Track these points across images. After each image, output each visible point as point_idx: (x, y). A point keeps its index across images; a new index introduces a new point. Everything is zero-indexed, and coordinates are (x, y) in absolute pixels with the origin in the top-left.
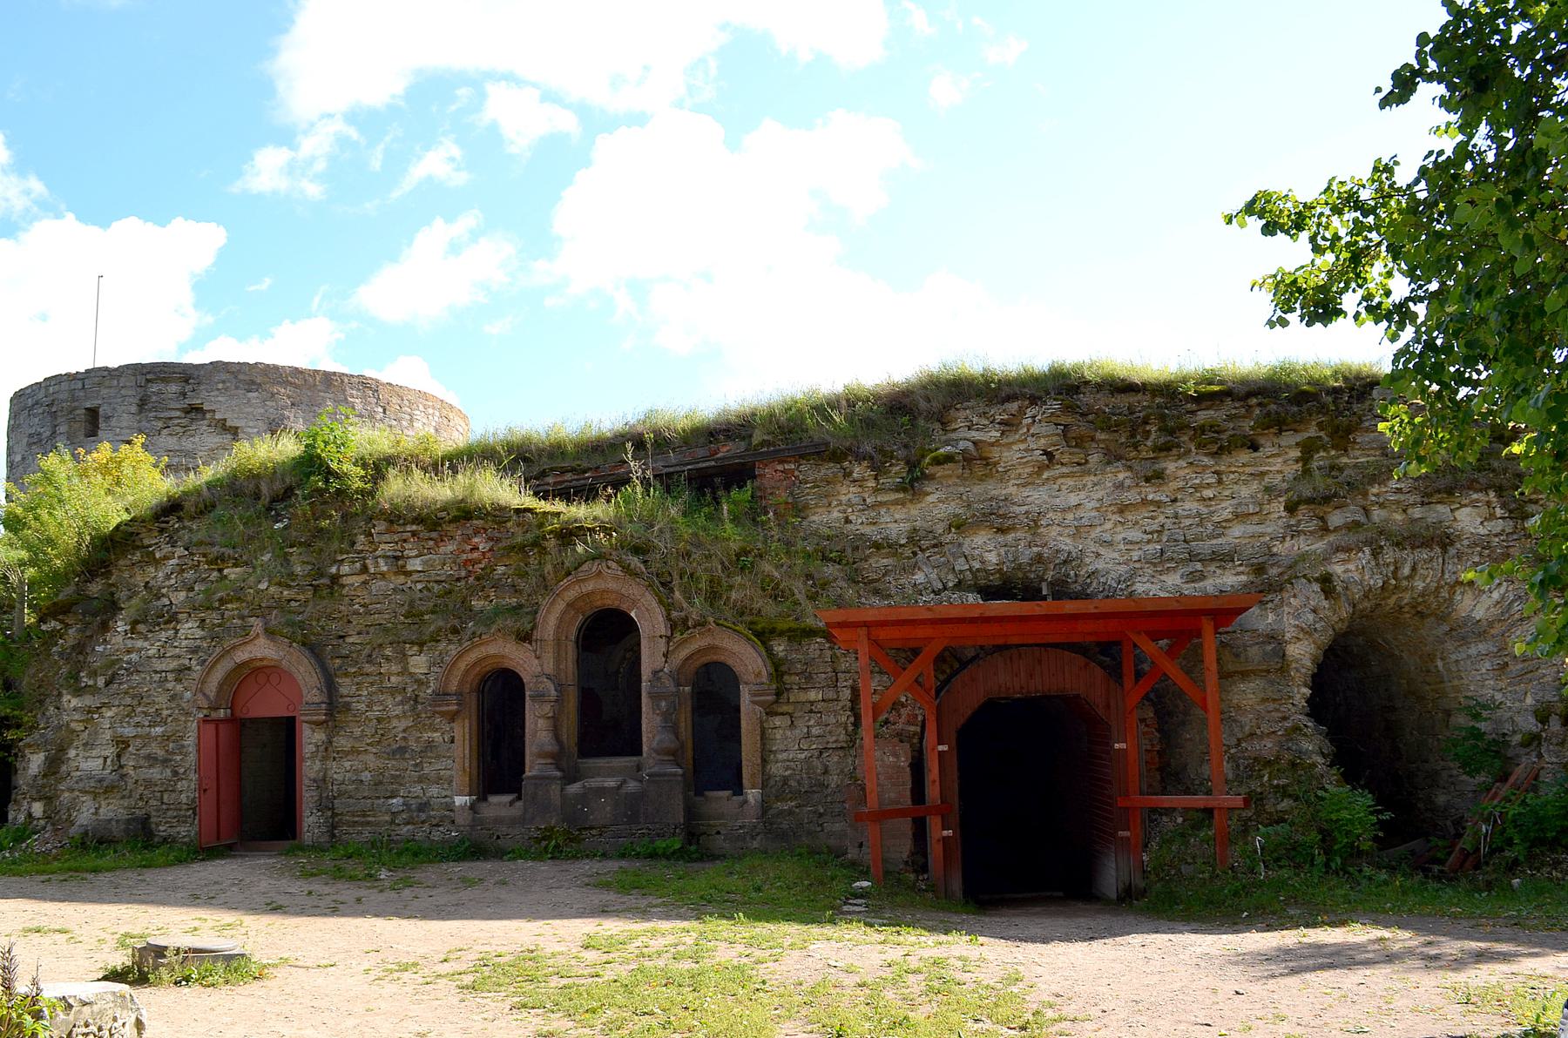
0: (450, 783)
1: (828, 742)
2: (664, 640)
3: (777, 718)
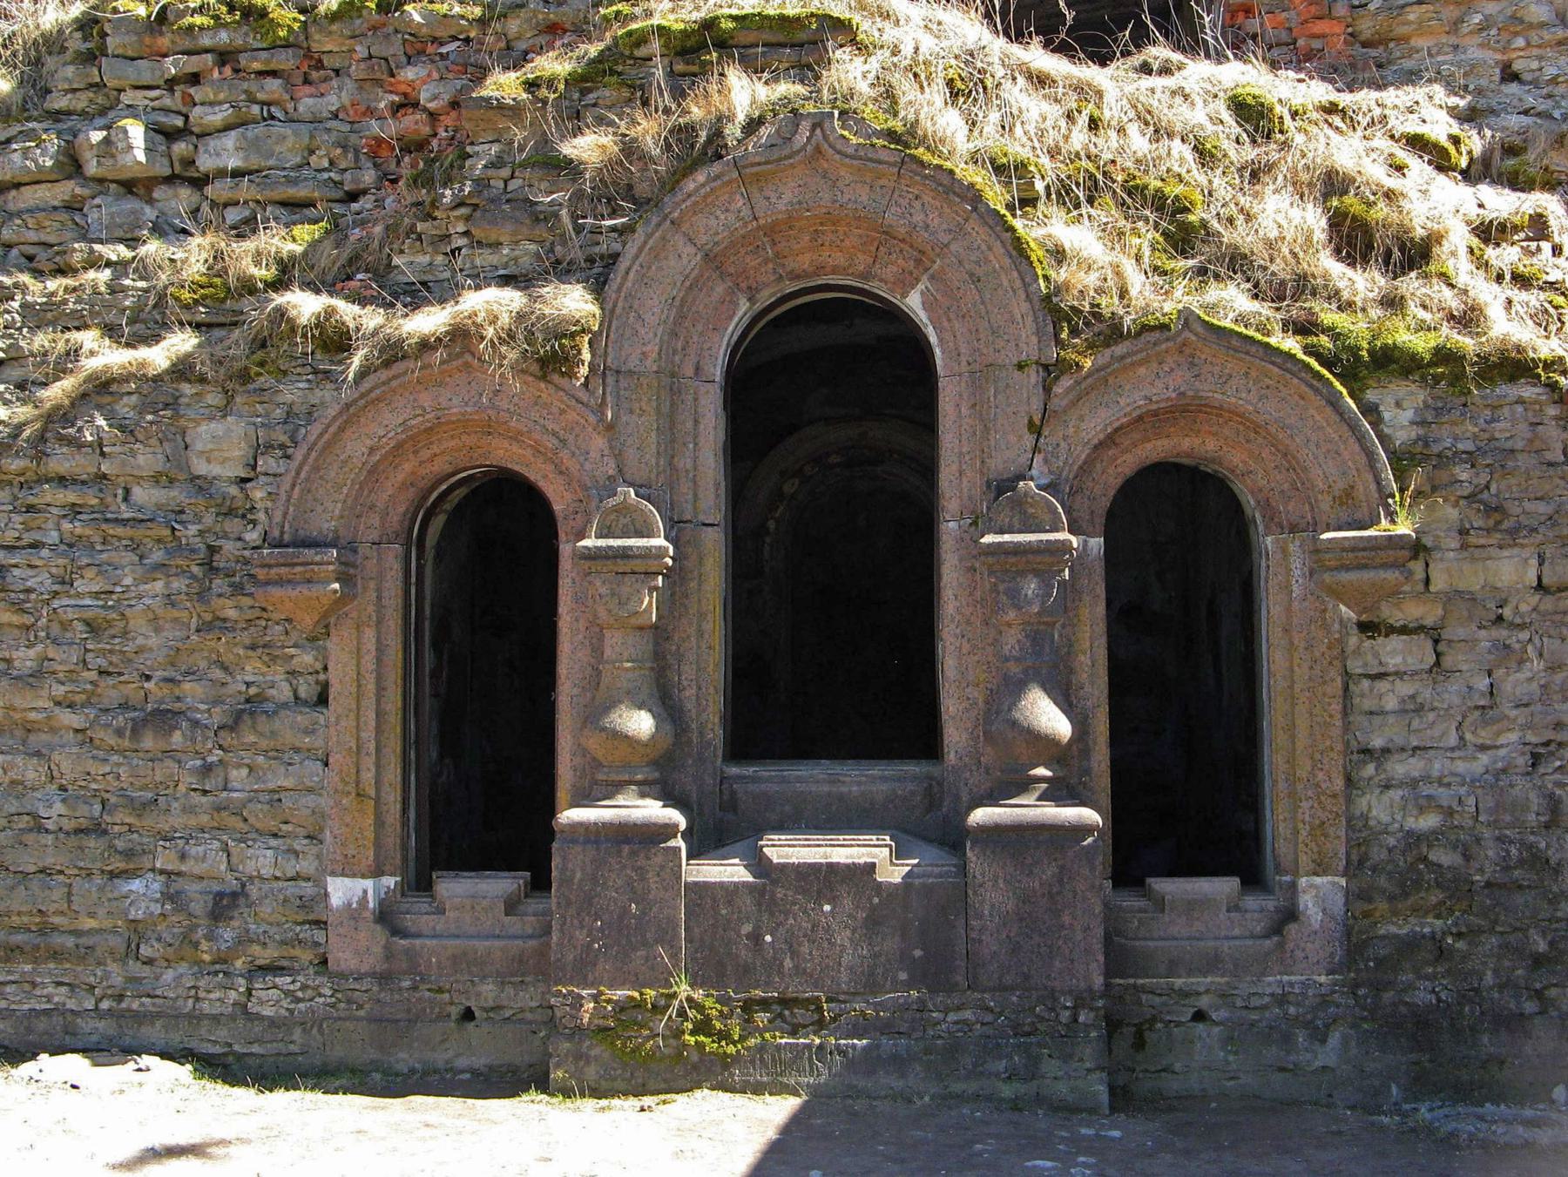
2: (1033, 376)
3: (1396, 641)
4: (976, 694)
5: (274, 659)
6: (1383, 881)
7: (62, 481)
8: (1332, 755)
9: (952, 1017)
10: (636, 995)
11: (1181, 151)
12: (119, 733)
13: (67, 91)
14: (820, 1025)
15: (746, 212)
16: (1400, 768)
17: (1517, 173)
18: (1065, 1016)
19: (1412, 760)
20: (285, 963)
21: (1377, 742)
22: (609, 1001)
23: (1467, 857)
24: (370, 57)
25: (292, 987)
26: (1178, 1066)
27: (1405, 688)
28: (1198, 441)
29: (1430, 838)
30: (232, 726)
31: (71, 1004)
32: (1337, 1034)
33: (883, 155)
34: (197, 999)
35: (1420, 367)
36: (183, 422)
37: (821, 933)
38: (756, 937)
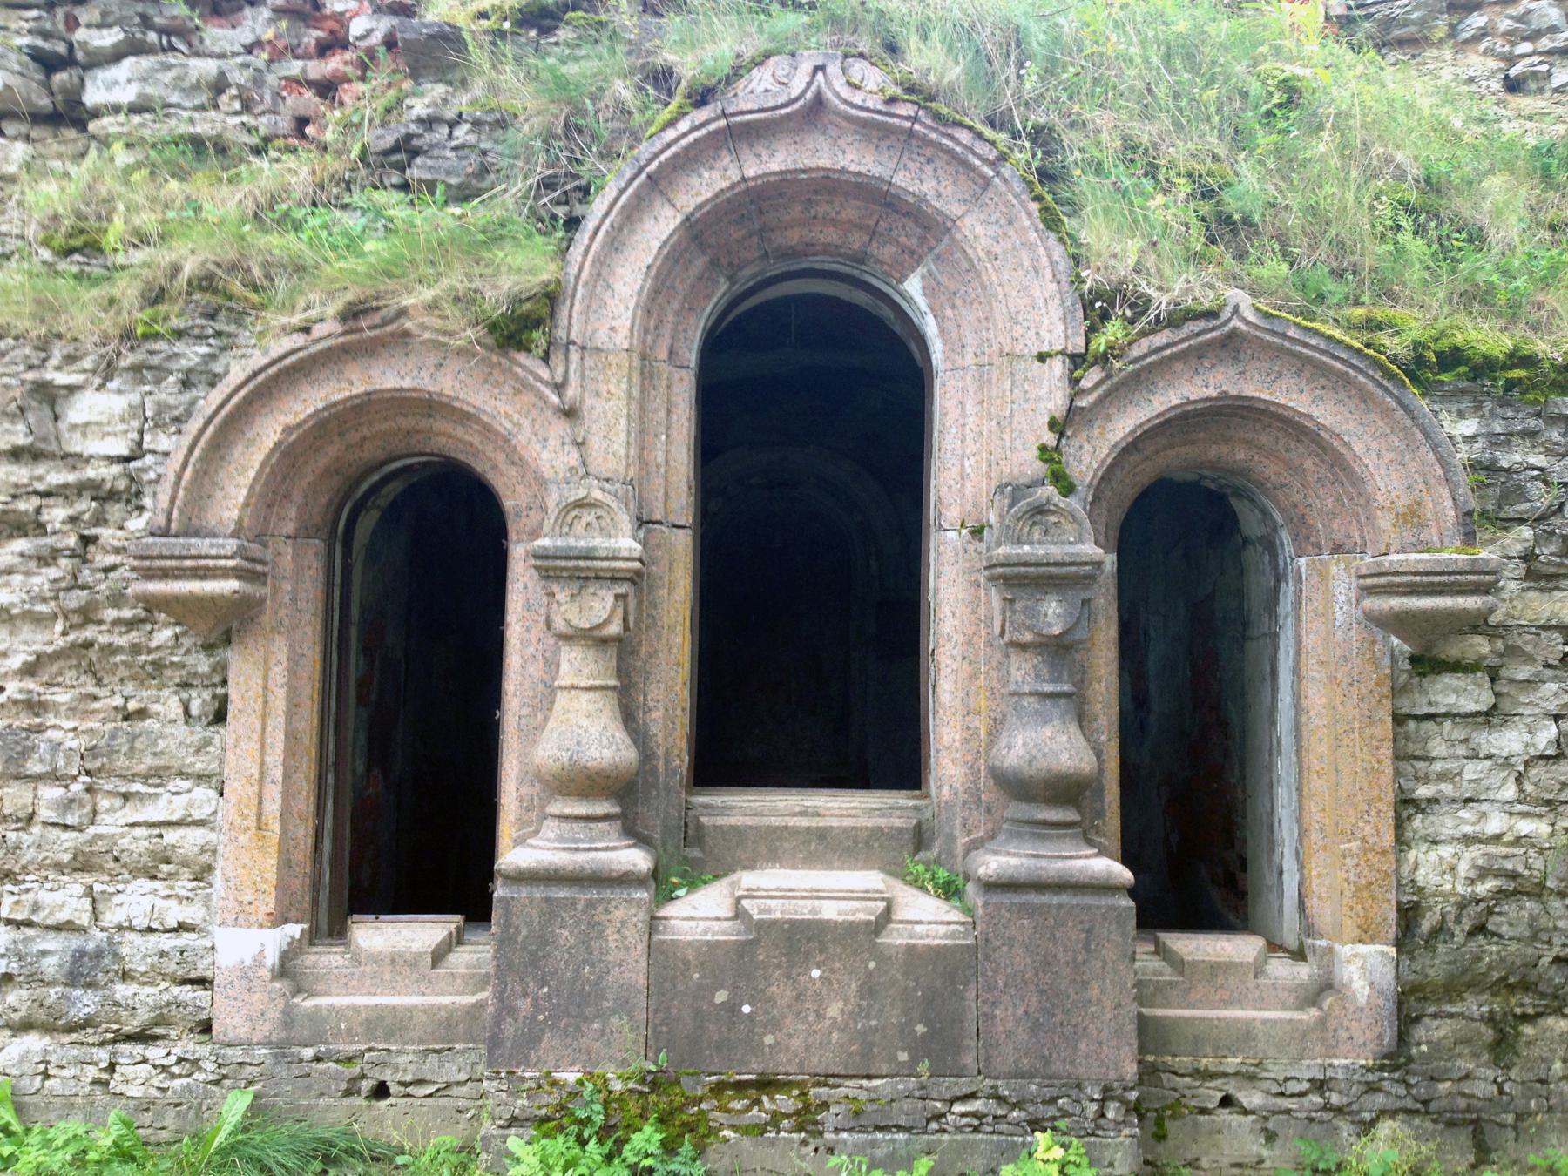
0: (202, 874)
2: (1058, 367)
4: (977, 723)
8: (1380, 806)
25: (165, 1062)
28: (1225, 449)
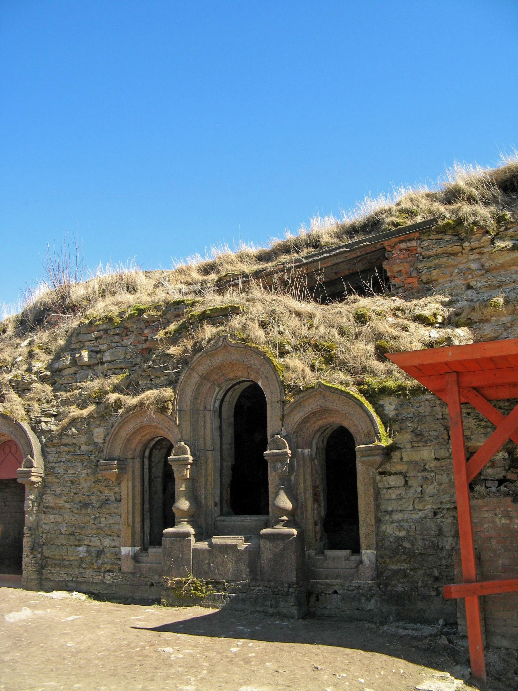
1: (441, 503)
3: (393, 477)
5: (111, 489)
6: (387, 552)
7: (66, 445)
9: (257, 588)
10: (181, 579)
11: (335, 332)
12: (78, 509)
13: (74, 344)
14: (224, 589)
15: (210, 364)
16: (397, 517)
17: (457, 322)
18: (286, 589)
19: (399, 514)
20: (112, 569)
21: (390, 509)
22: (174, 581)
23: (413, 545)
24: (137, 328)
26: (328, 607)
27: (397, 492)
28: (334, 419)
29: (402, 539)
30: (100, 507)
31: (67, 579)
32: (374, 599)
33: (240, 345)
34: (93, 578)
35: (394, 392)
36: (91, 429)
37: (224, 564)
38: (209, 564)
